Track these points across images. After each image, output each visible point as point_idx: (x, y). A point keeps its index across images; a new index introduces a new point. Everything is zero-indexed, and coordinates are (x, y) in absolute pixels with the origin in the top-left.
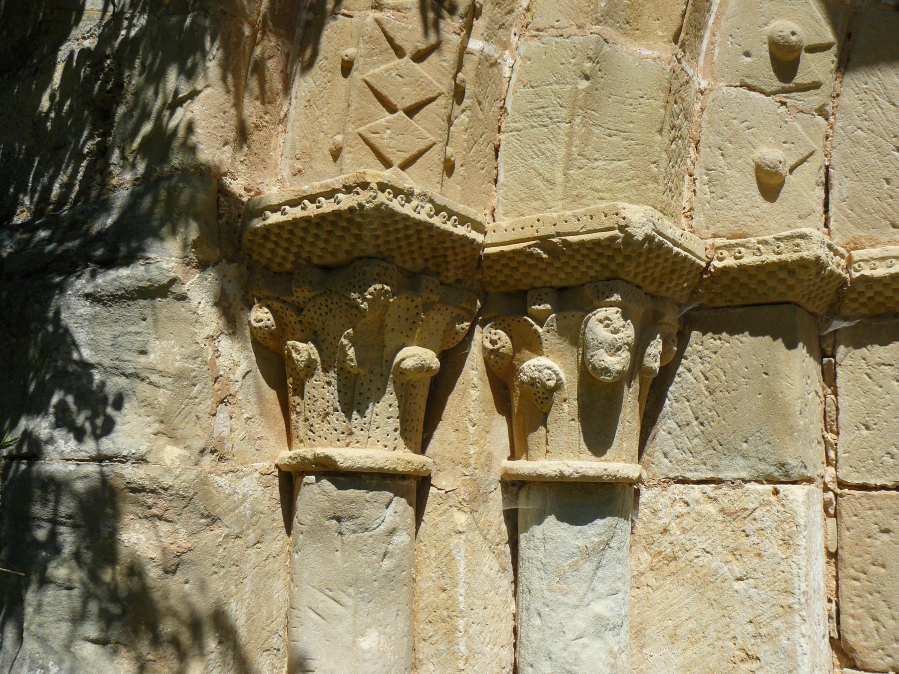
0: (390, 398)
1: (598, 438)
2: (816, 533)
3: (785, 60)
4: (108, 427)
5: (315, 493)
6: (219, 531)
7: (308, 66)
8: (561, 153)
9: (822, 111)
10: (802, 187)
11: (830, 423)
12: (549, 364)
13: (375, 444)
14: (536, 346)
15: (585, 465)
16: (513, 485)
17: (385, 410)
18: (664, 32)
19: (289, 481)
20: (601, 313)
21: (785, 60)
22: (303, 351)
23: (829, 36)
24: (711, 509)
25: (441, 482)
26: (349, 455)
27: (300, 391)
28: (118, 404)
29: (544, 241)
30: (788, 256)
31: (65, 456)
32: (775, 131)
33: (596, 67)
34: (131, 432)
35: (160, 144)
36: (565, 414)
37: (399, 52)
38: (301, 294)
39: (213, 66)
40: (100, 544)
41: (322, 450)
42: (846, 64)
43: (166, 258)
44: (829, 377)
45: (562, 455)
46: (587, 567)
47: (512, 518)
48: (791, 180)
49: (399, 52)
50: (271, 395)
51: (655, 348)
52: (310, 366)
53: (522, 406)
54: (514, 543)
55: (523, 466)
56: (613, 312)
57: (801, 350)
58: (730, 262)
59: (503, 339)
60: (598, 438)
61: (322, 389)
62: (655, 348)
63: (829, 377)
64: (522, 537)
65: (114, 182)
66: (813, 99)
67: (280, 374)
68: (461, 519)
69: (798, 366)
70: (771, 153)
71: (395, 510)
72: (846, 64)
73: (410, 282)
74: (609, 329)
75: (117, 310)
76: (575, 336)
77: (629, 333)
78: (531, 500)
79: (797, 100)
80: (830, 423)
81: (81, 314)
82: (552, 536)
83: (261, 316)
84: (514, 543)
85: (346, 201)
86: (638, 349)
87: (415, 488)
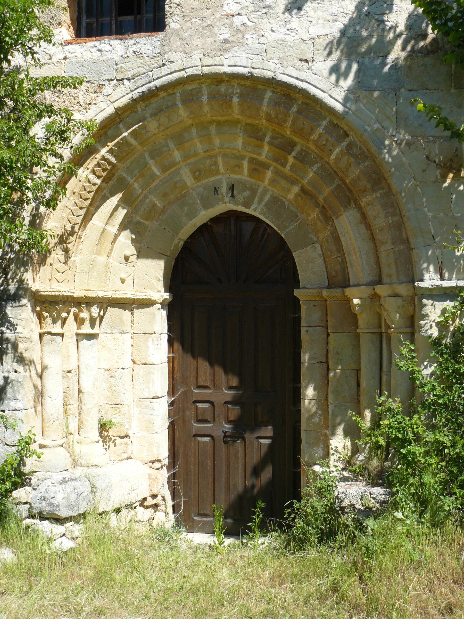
0: (60, 321)
1: (93, 326)
2: (130, 341)
3: (127, 259)
4: (16, 329)
5: (47, 338)
6: (33, 344)
7: (44, 265)
8: (87, 278)
9: (133, 266)
10: (129, 281)
11: (132, 323)
12: (84, 315)
13: (57, 329)
14: (82, 311)
15: (90, 331)
16: (77, 335)
17: (59, 323)
18: (105, 255)
19: (41, 336)
20: (94, 307)
21: (127, 259)
22: (46, 314)
23: (135, 252)
24: (111, 338)
25: (66, 334)
26: (54, 331)
27: (44, 320)
28: (17, 325)
29: (85, 296)
30: (125, 297)
31: (8, 334)
32: (125, 271)
33: (93, 263)
34: (19, 329)
35: (21, 281)
36: (87, 323)
37: (61, 262)
38: (45, 305)
39: (30, 271)
40: (15, 347)
41: (49, 330)
42: (138, 257)
43: (25, 301)
44: (132, 314)
45: (86, 329)
46: (91, 348)
47: (77, 340)
48: (127, 280)
49: (61, 262)
50: (38, 321)
51: (102, 312)
52: (47, 317)
53: (80, 322)
54: (78, 344)
55: (80, 331)
56: (96, 308)
57: (127, 311)
58: (115, 297)
59: (77, 311)
60: (93, 326)
61: (49, 320)
62: (102, 312)
63: (132, 314)
64: (79, 343)
65: (247, 435)
66: (132, 264)
67: (40, 317)
68: (70, 340)
69: (128, 313)
70: (124, 276)
71: (59, 339)
72: (138, 257)
73: (64, 303)
74: (95, 310)
75: (16, 308)
76: (89, 310)
77: (98, 310)
78: (80, 337)
79: (128, 265)
80: (132, 323)
81: (10, 311)
82: (84, 343)
83: (38, 308)
84: (78, 344)
85: (57, 293)
86: (99, 313)
87: (62, 335)
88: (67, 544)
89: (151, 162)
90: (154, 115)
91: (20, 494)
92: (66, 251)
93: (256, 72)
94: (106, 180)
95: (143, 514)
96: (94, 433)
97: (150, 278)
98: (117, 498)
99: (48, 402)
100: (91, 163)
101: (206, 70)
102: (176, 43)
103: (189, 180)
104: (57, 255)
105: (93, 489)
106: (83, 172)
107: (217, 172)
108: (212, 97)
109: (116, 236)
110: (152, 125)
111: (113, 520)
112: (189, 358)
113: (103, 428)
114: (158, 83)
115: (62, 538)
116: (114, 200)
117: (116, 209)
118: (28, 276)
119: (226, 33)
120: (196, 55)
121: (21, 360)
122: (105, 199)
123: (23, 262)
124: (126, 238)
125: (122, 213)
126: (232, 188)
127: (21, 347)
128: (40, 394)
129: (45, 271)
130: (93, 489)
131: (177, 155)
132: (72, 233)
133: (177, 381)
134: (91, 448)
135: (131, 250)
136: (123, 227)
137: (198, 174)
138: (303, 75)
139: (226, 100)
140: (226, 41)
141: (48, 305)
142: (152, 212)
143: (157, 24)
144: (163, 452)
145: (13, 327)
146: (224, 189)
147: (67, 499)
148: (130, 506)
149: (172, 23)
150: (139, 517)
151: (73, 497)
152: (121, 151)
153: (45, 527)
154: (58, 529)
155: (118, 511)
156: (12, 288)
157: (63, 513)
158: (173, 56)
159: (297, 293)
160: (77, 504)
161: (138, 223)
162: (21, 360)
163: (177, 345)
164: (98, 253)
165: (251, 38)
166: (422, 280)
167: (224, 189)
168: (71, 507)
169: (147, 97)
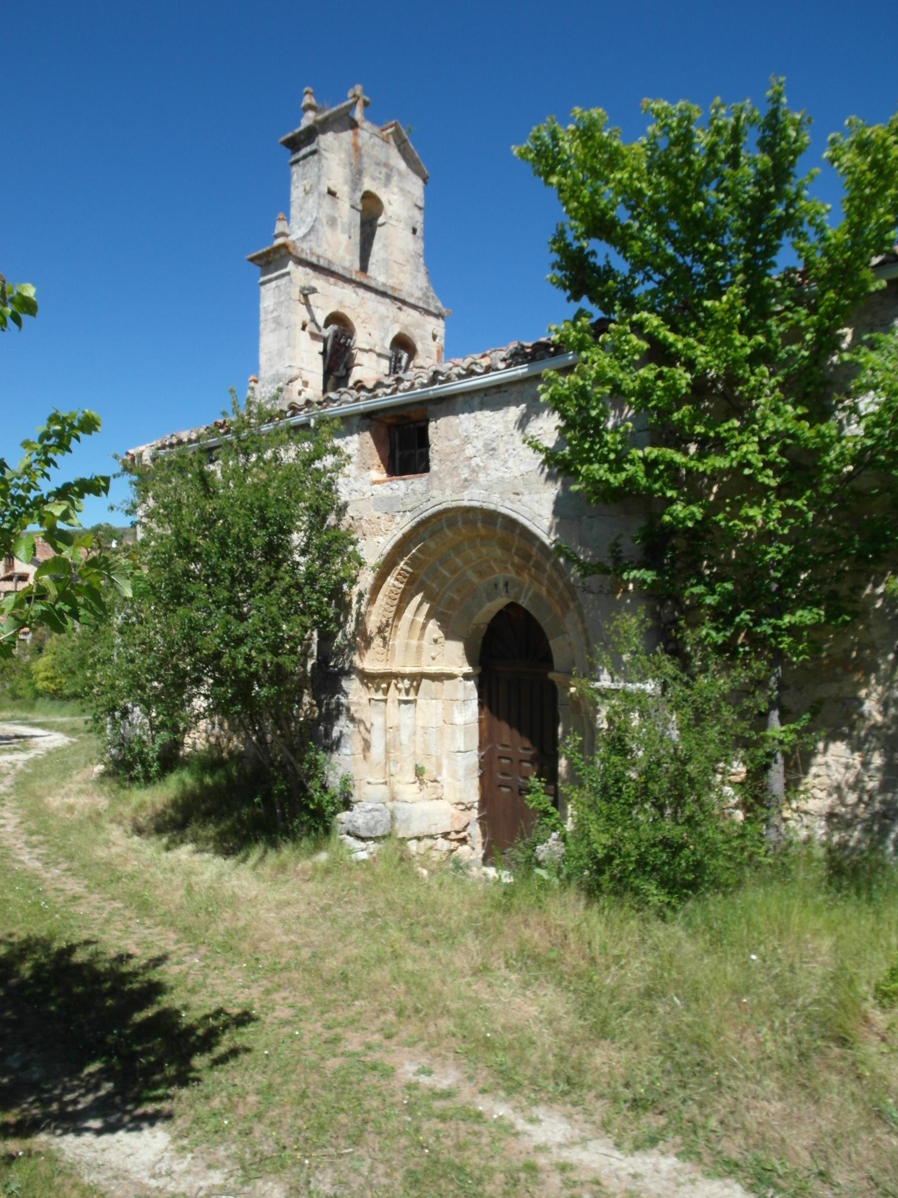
3: (436, 641)
31: (343, 700)
32: (434, 650)
40: (348, 710)
81: (344, 684)
88: (363, 855)
89: (441, 569)
90: (431, 536)
91: (343, 816)
92: (384, 638)
93: (485, 506)
94: (407, 584)
95: (443, 845)
96: (411, 777)
97: (453, 657)
98: (416, 828)
99: (373, 749)
100: (395, 573)
101: (454, 504)
102: (436, 482)
103: (475, 579)
104: (377, 642)
105: (393, 818)
106: (390, 580)
107: (494, 572)
108: (465, 522)
109: (424, 627)
110: (431, 544)
111: (413, 846)
112: (495, 720)
113: (419, 772)
114: (426, 514)
115: (362, 852)
116: (418, 598)
117: (421, 604)
118: (356, 658)
119: (465, 474)
120: (448, 492)
121: (352, 719)
122: (412, 597)
123: (352, 647)
124: (433, 625)
125: (426, 607)
126: (506, 584)
127: (353, 709)
128: (367, 745)
129: (369, 654)
130: (393, 818)
131: (459, 562)
132: (387, 625)
133: (486, 740)
134: (408, 789)
135: (439, 634)
136: (429, 616)
137: (481, 574)
138: (516, 507)
139: (474, 523)
140: (466, 480)
141: (369, 679)
142: (451, 603)
143: (427, 469)
144: (473, 795)
145: (346, 694)
146: (501, 586)
147: (367, 824)
148: (431, 837)
149: (434, 466)
150: (439, 846)
151: (372, 823)
152: (412, 563)
153: (350, 840)
154: (362, 845)
155: (419, 839)
156: (347, 666)
157: (363, 833)
158: (434, 493)
159: (551, 676)
160: (375, 828)
161: (442, 613)
162: (352, 719)
163: (486, 709)
164: (409, 637)
165: (482, 477)
166: (598, 680)
167: (501, 586)
168: (369, 830)
169: (423, 524)
